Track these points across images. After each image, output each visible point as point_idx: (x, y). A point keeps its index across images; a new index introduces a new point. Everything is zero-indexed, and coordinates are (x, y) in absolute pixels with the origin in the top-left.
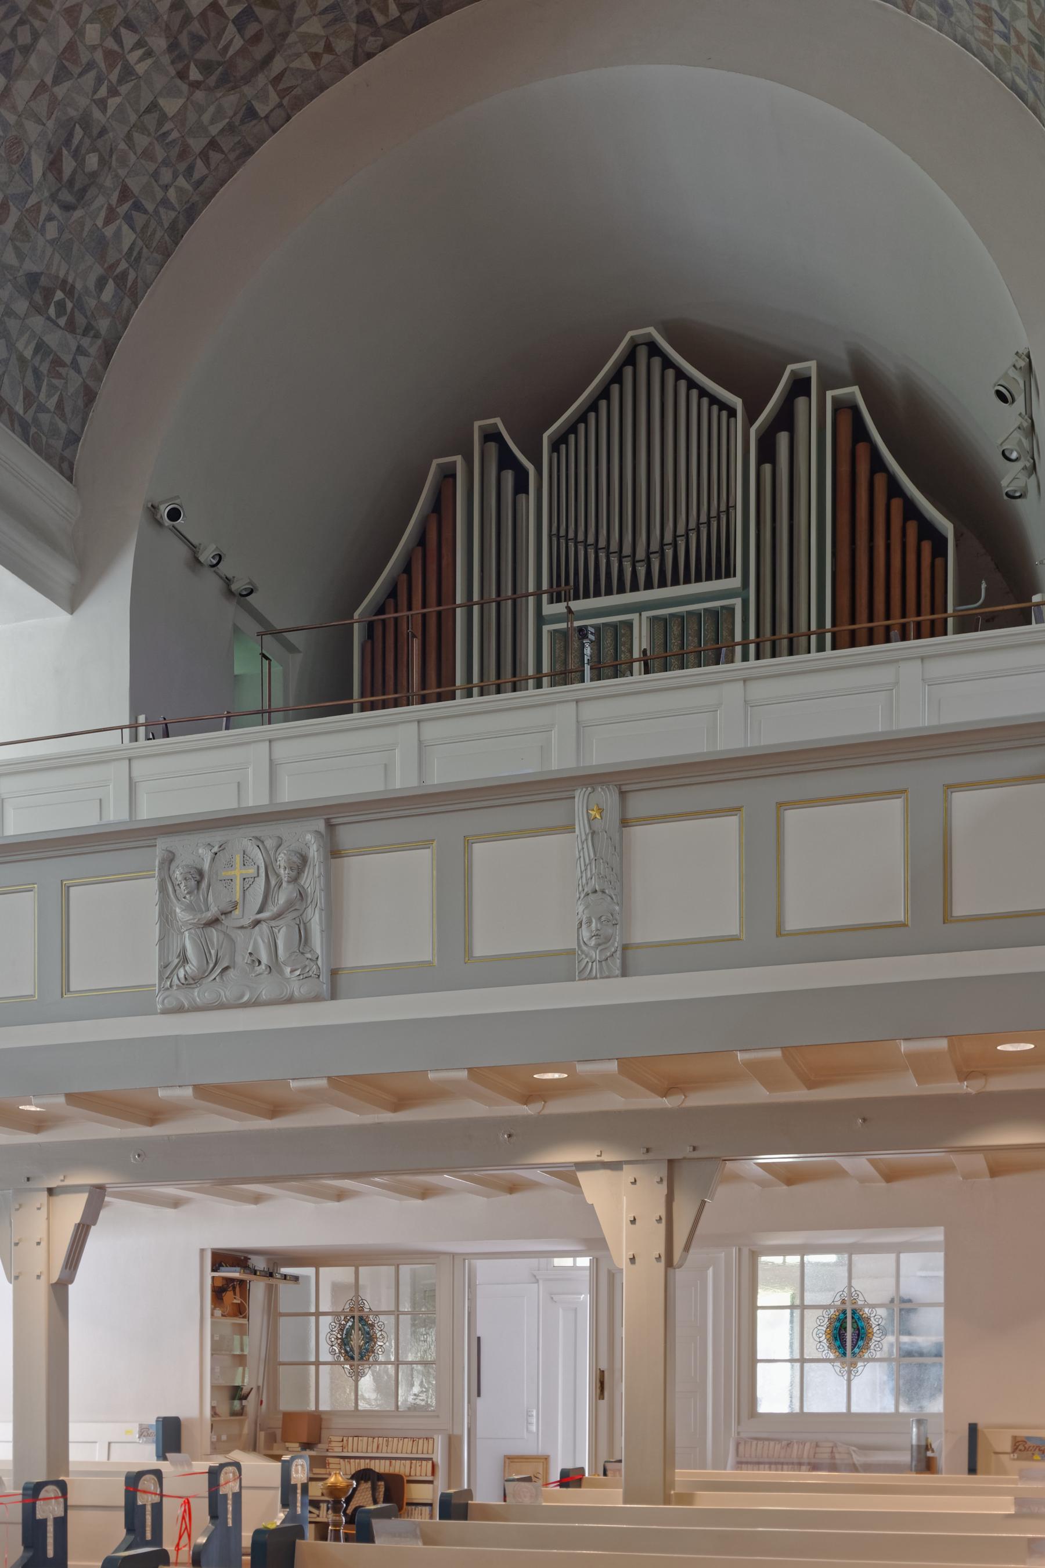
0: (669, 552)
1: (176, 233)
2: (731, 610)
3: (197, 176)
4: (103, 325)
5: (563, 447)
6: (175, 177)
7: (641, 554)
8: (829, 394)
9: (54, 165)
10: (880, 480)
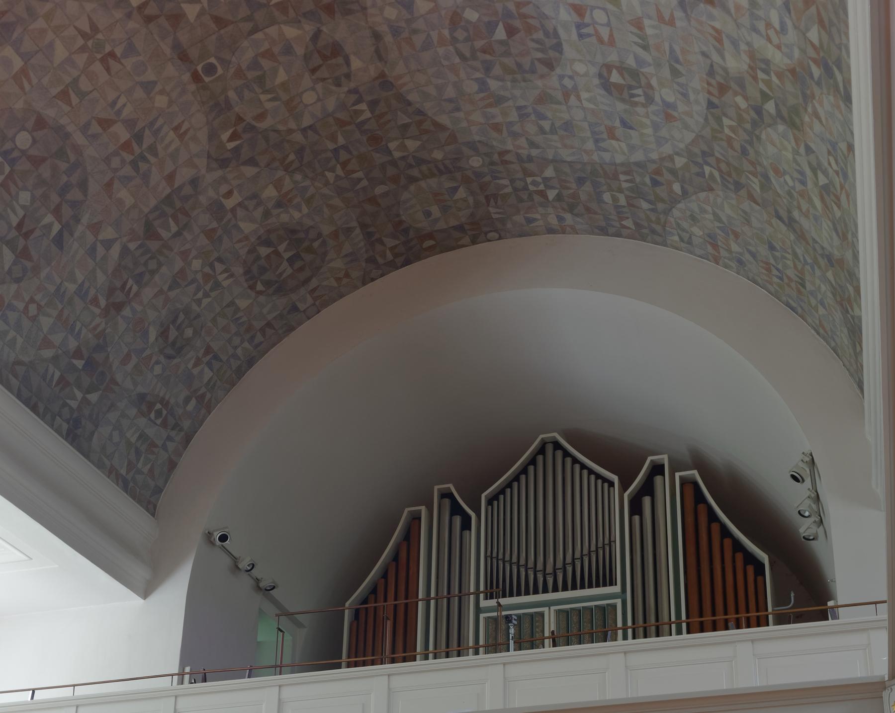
0: (569, 569)
1: (240, 373)
2: (614, 607)
3: (257, 341)
4: (186, 424)
5: (495, 503)
6: (242, 342)
7: (549, 569)
8: (677, 475)
9: (164, 334)
10: (715, 527)
